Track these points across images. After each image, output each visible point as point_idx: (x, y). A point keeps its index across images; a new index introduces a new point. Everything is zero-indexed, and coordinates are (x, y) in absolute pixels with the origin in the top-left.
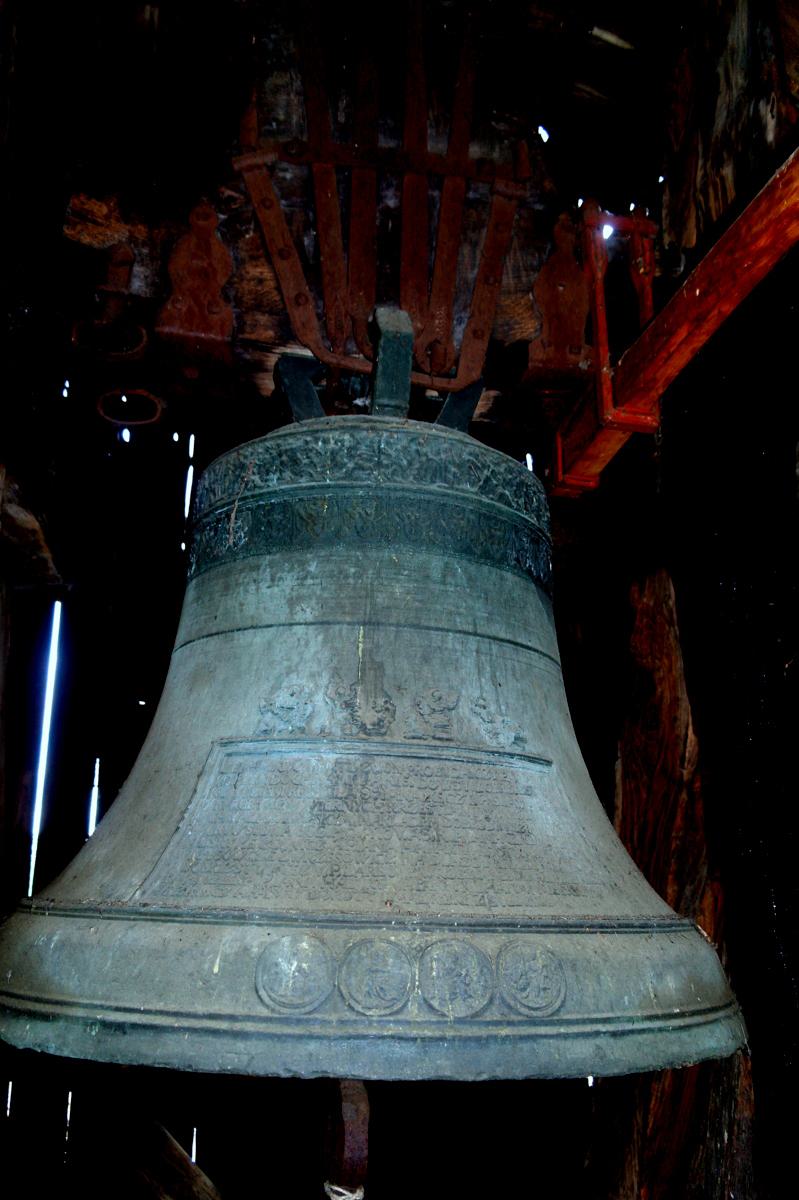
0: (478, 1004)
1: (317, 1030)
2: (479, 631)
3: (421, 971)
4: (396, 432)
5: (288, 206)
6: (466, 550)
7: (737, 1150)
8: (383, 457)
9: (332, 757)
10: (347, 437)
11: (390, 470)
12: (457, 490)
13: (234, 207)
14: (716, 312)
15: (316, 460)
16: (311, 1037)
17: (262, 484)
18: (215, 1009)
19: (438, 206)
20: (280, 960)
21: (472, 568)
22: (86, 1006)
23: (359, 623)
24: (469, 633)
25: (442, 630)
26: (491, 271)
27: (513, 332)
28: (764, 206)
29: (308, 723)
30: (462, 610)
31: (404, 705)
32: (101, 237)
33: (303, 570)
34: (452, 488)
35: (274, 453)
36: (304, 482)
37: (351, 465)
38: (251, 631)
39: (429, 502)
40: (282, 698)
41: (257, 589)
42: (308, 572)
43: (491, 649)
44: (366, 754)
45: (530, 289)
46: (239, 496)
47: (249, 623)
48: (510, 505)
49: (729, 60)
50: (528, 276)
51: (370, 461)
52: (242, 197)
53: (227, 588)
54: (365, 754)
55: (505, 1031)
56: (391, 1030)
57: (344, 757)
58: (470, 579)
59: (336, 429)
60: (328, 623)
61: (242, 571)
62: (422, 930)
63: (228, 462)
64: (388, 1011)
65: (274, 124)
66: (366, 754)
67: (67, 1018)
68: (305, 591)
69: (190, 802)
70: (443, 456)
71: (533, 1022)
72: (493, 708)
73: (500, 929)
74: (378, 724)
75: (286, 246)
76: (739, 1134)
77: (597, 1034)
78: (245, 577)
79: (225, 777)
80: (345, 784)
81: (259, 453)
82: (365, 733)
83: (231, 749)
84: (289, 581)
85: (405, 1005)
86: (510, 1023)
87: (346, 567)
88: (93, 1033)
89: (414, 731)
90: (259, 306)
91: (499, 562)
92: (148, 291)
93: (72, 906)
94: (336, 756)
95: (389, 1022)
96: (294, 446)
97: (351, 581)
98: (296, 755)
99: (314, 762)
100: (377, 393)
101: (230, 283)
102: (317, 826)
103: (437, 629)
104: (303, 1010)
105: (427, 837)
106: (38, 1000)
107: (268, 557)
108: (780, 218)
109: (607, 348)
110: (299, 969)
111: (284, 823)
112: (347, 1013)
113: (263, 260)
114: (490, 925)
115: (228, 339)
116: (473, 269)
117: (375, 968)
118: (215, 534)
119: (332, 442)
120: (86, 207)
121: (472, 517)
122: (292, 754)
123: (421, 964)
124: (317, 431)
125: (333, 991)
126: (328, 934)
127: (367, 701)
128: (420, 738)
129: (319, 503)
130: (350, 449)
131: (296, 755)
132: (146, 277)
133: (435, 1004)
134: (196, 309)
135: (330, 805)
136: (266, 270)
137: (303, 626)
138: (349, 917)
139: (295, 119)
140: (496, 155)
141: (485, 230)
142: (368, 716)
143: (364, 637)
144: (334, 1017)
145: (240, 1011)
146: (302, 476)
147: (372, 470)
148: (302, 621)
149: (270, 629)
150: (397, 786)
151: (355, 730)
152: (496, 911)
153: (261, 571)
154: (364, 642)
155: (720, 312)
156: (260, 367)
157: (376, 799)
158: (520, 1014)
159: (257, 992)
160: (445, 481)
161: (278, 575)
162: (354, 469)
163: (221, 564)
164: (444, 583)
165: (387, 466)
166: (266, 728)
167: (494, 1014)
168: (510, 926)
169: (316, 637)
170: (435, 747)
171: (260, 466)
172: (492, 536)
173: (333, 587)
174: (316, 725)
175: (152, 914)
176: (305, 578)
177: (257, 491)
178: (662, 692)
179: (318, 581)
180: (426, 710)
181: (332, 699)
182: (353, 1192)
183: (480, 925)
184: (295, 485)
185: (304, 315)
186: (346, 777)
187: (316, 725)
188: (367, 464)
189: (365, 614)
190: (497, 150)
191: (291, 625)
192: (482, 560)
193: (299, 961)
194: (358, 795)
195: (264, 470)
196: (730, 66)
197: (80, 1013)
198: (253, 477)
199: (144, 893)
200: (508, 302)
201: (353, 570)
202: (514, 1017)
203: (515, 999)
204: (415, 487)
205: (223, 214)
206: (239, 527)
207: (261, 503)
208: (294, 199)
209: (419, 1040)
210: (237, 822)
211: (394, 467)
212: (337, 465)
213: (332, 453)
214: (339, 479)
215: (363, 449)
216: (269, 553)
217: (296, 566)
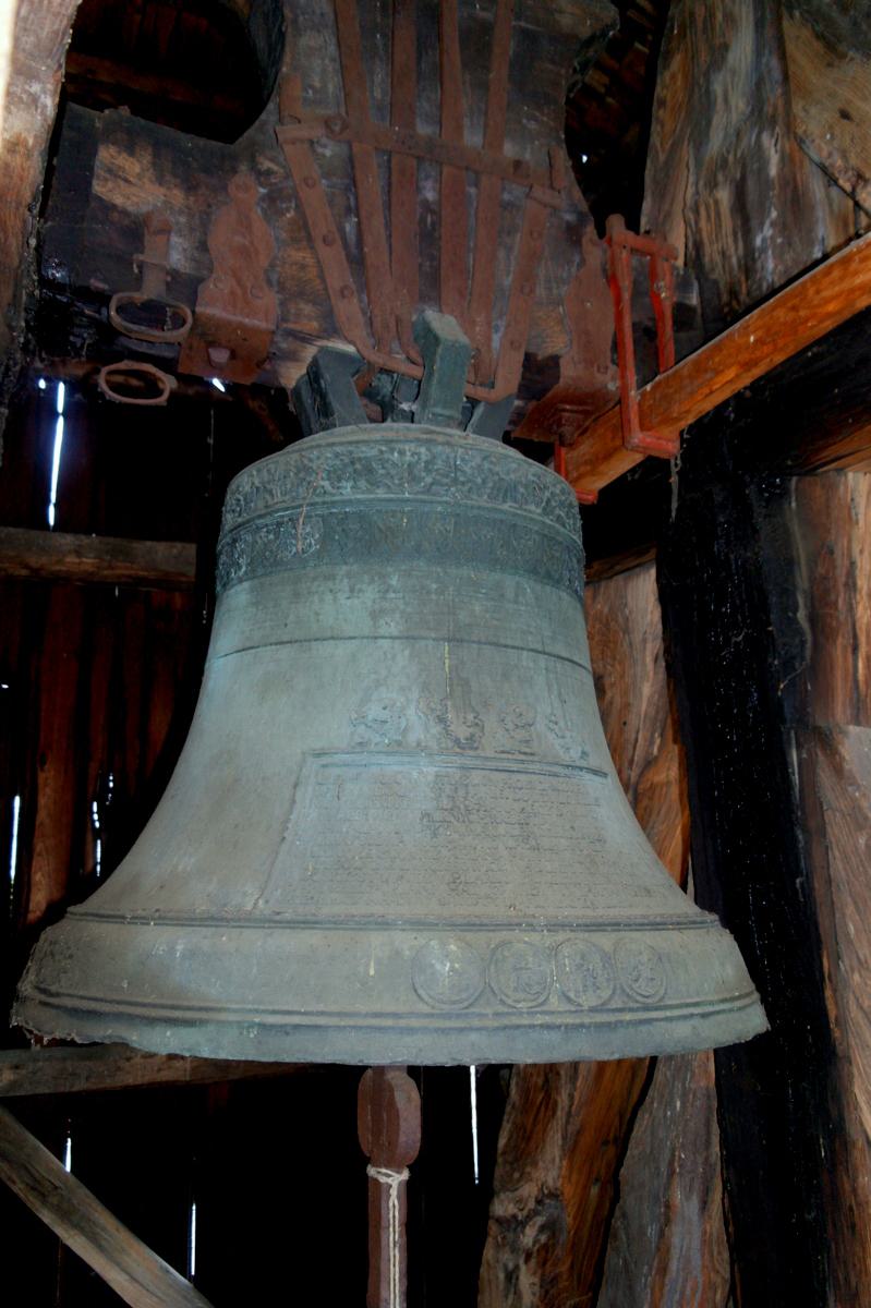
0: (606, 994)
1: (476, 1023)
2: (547, 650)
3: (557, 967)
4: (471, 449)
5: (328, 186)
6: (533, 571)
7: (691, 1116)
8: (459, 473)
9: (432, 770)
10: (423, 450)
11: (466, 488)
12: (525, 510)
13: (273, 181)
14: (768, 360)
15: (393, 472)
16: (471, 1029)
17: (334, 491)
18: (377, 1008)
19: (475, 204)
20: (433, 962)
21: (538, 587)
22: (235, 1011)
23: (444, 639)
24: (540, 652)
25: (517, 648)
26: (526, 279)
27: (545, 345)
28: (836, 274)
29: (404, 737)
30: (532, 629)
31: (490, 722)
32: (135, 199)
33: (385, 583)
34: (521, 508)
35: (347, 460)
36: (381, 493)
37: (429, 480)
38: (332, 642)
39: (502, 521)
40: (374, 711)
41: (335, 599)
42: (390, 586)
43: (555, 667)
44: (463, 768)
45: (559, 302)
46: (307, 501)
47: (329, 634)
48: (564, 526)
49: (729, 80)
50: (558, 288)
51: (447, 476)
52: (282, 171)
53: (297, 595)
54: (462, 768)
55: (628, 1017)
56: (539, 1020)
57: (444, 770)
58: (537, 599)
59: (411, 441)
60: (414, 638)
61: (315, 579)
62: (549, 931)
63: (287, 463)
64: (534, 1003)
65: (310, 92)
66: (463, 768)
67: (219, 1022)
68: (387, 605)
69: (291, 812)
70: (512, 476)
71: (647, 1008)
72: (562, 724)
73: (609, 928)
74: (471, 739)
75: (329, 231)
76: (693, 1101)
77: (692, 1015)
78: (319, 586)
79: (324, 788)
80: (449, 796)
81: (327, 458)
82: (459, 747)
83: (325, 760)
84: (370, 594)
85: (547, 999)
86: (631, 1010)
87: (428, 582)
88: (252, 1035)
89: (503, 746)
90: (301, 294)
91: (557, 583)
92: (187, 265)
93: (186, 916)
94: (436, 769)
95: (537, 1013)
96: (369, 455)
97: (434, 597)
98: (396, 768)
99: (415, 774)
100: (432, 401)
101: (273, 266)
102: (429, 837)
103: (513, 647)
104: (461, 1006)
105: (528, 846)
106: (173, 1007)
107: (344, 568)
108: (852, 291)
109: (633, 370)
110: (452, 969)
111: (396, 833)
112: (500, 1006)
113: (305, 243)
114: (600, 925)
115: (273, 327)
116: (508, 275)
117: (518, 966)
118: (276, 538)
119: (408, 454)
120: (116, 162)
121: (537, 538)
122: (392, 766)
123: (557, 962)
124: (392, 441)
125: (485, 988)
126: (469, 936)
127: (458, 717)
128: (509, 753)
129: (399, 515)
130: (426, 462)
131: (396, 768)
132: (185, 250)
133: (572, 995)
134: (239, 292)
135: (438, 816)
136: (309, 255)
137: (388, 640)
138: (485, 921)
139: (331, 87)
140: (528, 156)
141: (519, 235)
142: (462, 732)
143: (449, 653)
144: (489, 1011)
145: (402, 1009)
146: (378, 487)
147: (450, 487)
148: (387, 635)
149: (353, 641)
150: (496, 798)
151: (450, 744)
152: (600, 912)
153: (337, 581)
154: (450, 658)
155: (771, 360)
156: (292, 357)
157: (478, 811)
158: (637, 1002)
159: (416, 991)
160: (515, 502)
161: (358, 586)
162: (432, 484)
163: (286, 570)
164: (516, 602)
165: (463, 484)
166: (360, 740)
167: (617, 1003)
168: (616, 926)
169: (403, 651)
170: (523, 762)
171: (329, 472)
172: (553, 557)
173: (416, 602)
174: (412, 738)
175: (288, 922)
176: (387, 591)
177: (328, 498)
178: (612, 698)
179: (401, 595)
180: (510, 726)
181: (423, 713)
182: (399, 1172)
183: (594, 925)
184: (372, 496)
185: (349, 309)
186: (448, 790)
187: (412, 738)
188: (445, 480)
189: (449, 630)
190: (529, 150)
191: (376, 638)
192: (545, 581)
193: (452, 962)
194: (462, 806)
195: (336, 476)
196: (730, 87)
197: (232, 1017)
198: (322, 483)
199: (267, 902)
200: (541, 314)
201: (434, 586)
202: (632, 1005)
203: (632, 989)
204: (490, 505)
205: (264, 188)
206: (308, 534)
207: (334, 510)
208: (334, 180)
209: (563, 1028)
210: (347, 832)
211: (470, 485)
212: (414, 479)
213: (409, 465)
214: (418, 493)
215: (439, 464)
216: (346, 563)
217: (376, 578)
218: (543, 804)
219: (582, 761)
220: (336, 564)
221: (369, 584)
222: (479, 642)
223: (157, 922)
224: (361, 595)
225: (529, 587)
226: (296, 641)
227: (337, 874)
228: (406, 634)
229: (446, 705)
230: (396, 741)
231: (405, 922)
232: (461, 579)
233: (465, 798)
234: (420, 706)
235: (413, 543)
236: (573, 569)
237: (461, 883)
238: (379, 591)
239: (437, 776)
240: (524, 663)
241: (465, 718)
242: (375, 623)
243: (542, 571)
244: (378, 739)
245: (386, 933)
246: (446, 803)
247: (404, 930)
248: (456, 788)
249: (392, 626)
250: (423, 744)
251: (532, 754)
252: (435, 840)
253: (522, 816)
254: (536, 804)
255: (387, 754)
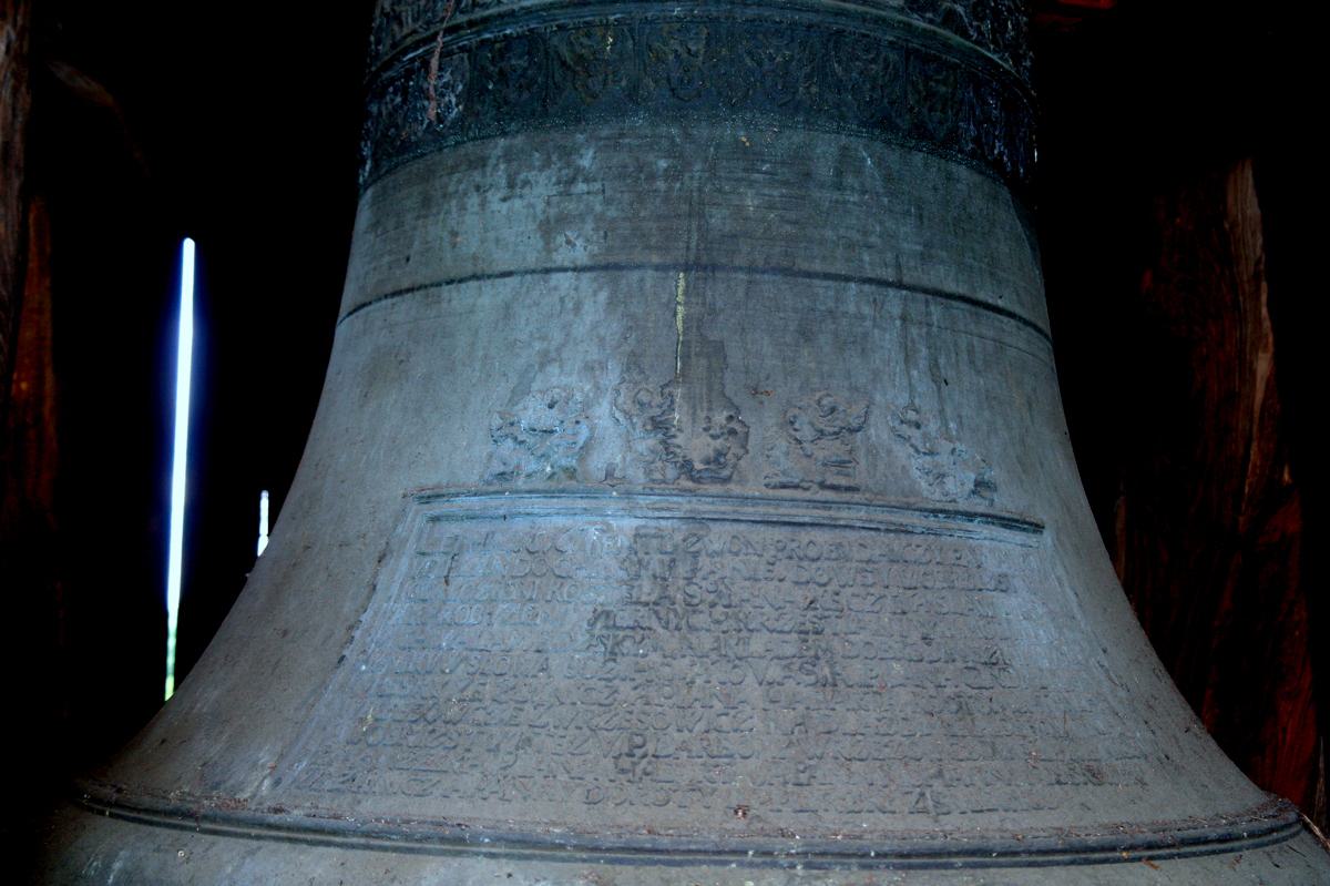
2: (906, 280)
6: (881, 123)
9: (629, 524)
21: (894, 157)
23: (676, 267)
29: (582, 459)
30: (873, 239)
33: (568, 165)
38: (473, 284)
41: (483, 204)
42: (578, 170)
43: (929, 314)
47: (469, 269)
53: (426, 202)
57: (652, 523)
60: (618, 267)
62: (808, 866)
72: (933, 426)
73: (958, 861)
74: (716, 461)
78: (460, 182)
79: (427, 562)
83: (438, 508)
84: (542, 187)
87: (651, 157)
91: (944, 145)
97: (661, 185)
98: (560, 521)
99: (593, 534)
102: (600, 658)
103: (827, 276)
107: (502, 142)
121: (893, 57)
122: (552, 518)
128: (796, 487)
129: (599, 32)
131: (560, 521)
135: (625, 617)
138: (665, 842)
142: (697, 445)
143: (686, 293)
149: (507, 280)
151: (671, 473)
153: (489, 169)
157: (713, 605)
161: (522, 176)
164: (839, 187)
166: (502, 469)
169: (595, 293)
170: (826, 504)
172: (931, 94)
174: (597, 463)
176: (572, 181)
179: (597, 186)
180: (807, 433)
181: (625, 412)
186: (655, 563)
187: (597, 463)
189: (688, 248)
191: (548, 271)
201: (663, 164)
206: (446, 85)
207: (487, 36)
216: (504, 134)
217: (554, 158)
218: (862, 591)
219: (977, 500)
220: (489, 136)
221: (541, 169)
222: (751, 270)
223: (114, 811)
224: (526, 190)
225: (869, 156)
226: (419, 288)
227: (412, 732)
228: (602, 261)
229: (670, 394)
230: (566, 470)
231: (497, 840)
232: (718, 146)
233: (689, 581)
234: (621, 400)
235: (624, 83)
236: (988, 119)
237: (644, 756)
238: (558, 183)
239: (637, 535)
240: (852, 308)
241: (709, 419)
242: (547, 243)
243: (905, 123)
244: (533, 466)
245: (455, 863)
246: (647, 590)
247: (492, 856)
248: (673, 561)
249: (578, 248)
250: (618, 474)
251: (849, 489)
252: (611, 665)
253: (810, 614)
254: (849, 591)
255: (548, 493)
